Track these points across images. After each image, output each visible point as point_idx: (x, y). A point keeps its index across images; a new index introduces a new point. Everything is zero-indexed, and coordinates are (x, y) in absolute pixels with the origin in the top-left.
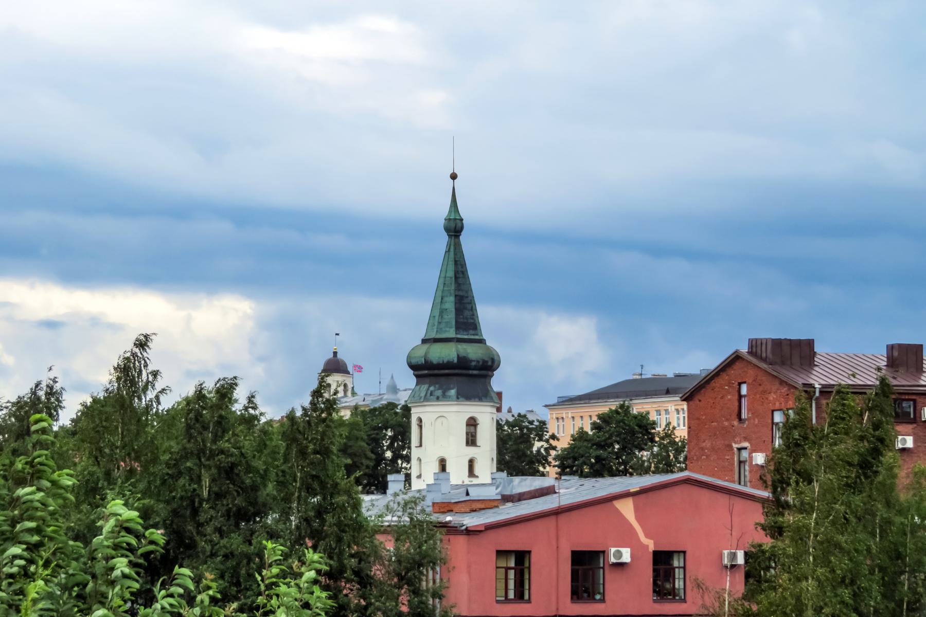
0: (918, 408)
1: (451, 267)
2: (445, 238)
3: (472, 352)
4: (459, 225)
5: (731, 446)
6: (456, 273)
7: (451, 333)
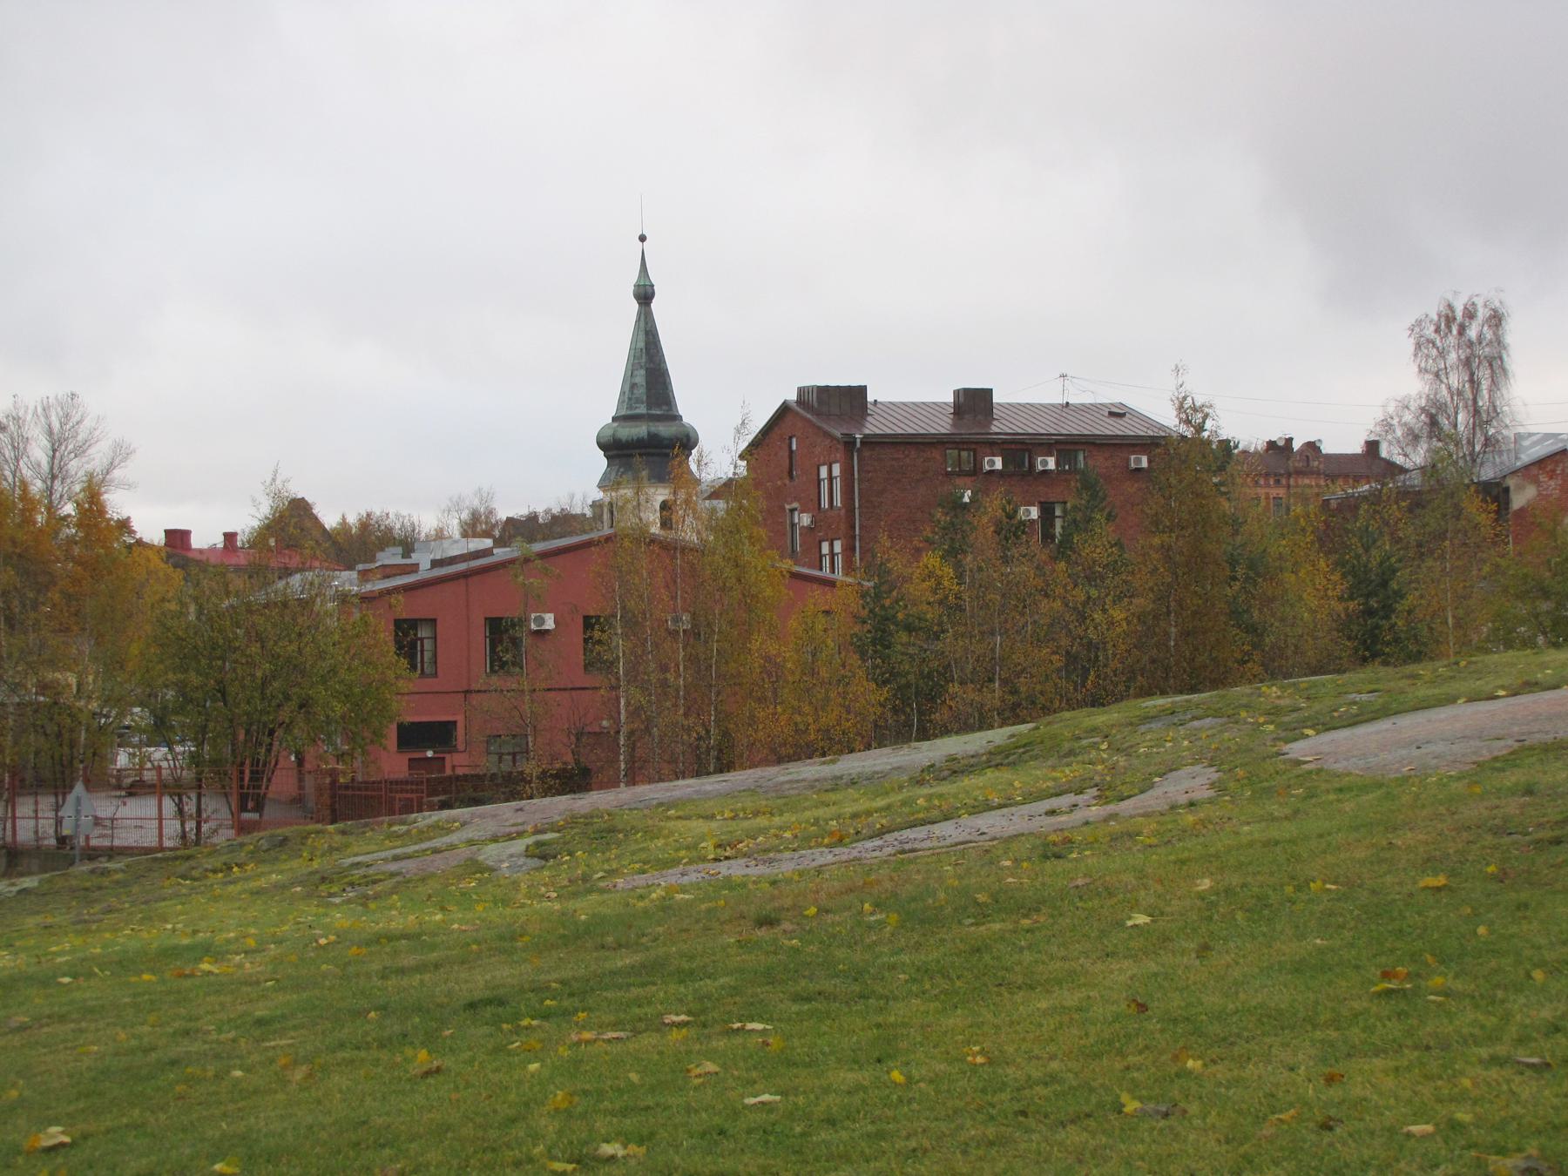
0: (979, 458)
1: (642, 337)
2: (635, 306)
3: (664, 430)
4: (650, 291)
5: (784, 509)
6: (647, 344)
7: (642, 410)
